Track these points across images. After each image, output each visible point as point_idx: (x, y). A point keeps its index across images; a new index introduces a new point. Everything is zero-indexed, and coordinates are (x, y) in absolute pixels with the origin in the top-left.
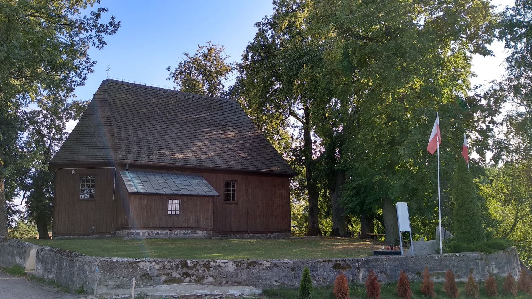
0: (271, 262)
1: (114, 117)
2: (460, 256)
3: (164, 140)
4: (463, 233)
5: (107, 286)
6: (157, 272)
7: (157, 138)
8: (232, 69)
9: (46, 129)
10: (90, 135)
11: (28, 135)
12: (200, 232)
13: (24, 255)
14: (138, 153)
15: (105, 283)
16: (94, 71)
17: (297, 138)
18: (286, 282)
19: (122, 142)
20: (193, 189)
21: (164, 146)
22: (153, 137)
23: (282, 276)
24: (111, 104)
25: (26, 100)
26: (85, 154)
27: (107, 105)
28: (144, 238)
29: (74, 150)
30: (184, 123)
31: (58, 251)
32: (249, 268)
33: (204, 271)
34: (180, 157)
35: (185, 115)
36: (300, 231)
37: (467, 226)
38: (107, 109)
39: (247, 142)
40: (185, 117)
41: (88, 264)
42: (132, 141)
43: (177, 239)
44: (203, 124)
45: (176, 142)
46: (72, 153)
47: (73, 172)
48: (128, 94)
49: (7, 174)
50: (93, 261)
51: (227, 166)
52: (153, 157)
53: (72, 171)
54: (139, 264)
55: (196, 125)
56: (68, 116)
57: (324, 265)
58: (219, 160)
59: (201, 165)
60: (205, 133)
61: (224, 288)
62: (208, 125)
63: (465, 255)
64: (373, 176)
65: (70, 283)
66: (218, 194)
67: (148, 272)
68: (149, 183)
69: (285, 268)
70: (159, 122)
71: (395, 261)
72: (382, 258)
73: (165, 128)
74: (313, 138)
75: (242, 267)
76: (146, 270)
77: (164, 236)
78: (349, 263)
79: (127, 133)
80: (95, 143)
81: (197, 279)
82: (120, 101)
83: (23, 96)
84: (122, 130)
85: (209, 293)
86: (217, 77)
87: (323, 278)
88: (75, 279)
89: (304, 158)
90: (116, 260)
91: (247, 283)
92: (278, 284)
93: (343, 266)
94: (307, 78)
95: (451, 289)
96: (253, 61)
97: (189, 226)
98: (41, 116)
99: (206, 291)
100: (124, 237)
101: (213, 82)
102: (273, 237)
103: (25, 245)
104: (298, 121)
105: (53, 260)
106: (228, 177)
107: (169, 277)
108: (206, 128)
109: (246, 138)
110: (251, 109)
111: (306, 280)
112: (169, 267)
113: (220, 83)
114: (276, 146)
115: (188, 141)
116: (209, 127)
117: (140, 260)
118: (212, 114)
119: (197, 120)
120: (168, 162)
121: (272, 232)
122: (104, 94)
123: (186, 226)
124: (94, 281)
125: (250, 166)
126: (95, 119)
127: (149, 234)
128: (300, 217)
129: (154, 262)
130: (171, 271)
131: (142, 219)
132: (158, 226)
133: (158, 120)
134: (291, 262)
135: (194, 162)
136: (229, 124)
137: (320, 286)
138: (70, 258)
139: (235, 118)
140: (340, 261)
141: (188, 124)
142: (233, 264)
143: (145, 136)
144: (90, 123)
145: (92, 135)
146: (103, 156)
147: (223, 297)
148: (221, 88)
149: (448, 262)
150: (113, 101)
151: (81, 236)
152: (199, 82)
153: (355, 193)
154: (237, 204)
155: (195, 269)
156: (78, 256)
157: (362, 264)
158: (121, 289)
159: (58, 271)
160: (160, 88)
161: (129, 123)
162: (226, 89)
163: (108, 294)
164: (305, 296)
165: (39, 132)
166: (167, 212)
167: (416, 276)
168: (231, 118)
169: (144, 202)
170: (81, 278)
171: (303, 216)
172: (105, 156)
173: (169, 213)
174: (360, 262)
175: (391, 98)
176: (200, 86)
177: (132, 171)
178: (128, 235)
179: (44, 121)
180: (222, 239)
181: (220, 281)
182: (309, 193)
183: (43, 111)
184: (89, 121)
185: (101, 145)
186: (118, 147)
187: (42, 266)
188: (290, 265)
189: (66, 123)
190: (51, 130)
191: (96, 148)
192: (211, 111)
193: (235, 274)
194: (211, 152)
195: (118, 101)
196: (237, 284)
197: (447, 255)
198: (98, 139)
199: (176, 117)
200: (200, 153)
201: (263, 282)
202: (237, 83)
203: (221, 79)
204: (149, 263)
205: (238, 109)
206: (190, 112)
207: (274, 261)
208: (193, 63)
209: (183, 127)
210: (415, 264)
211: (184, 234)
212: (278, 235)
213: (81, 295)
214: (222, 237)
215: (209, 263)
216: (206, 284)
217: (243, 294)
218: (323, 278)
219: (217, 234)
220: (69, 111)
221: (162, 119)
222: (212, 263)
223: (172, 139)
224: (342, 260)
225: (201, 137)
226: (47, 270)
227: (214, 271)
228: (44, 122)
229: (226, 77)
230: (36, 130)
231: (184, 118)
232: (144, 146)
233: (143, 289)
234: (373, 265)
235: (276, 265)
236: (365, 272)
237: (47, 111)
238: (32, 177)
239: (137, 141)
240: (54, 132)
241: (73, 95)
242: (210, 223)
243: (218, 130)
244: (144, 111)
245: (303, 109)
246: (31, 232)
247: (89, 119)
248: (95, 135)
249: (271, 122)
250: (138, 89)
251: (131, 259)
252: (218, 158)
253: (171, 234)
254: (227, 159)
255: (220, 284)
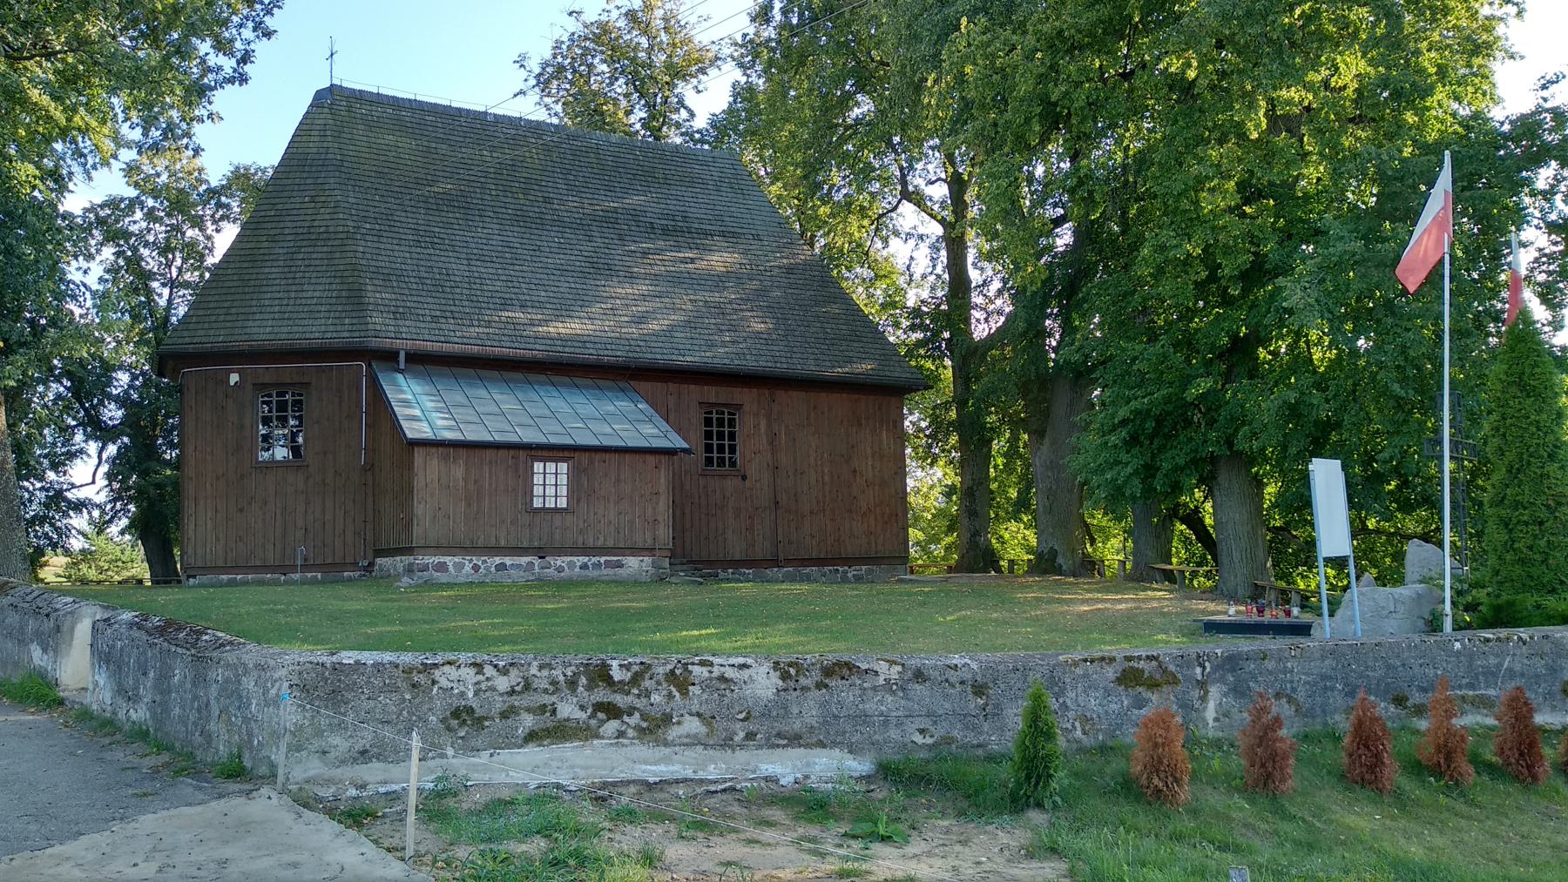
0: (903, 665)
1: (355, 206)
2: (1531, 638)
3: (514, 279)
4: (1522, 561)
5: (324, 753)
6: (504, 702)
7: (491, 270)
8: (717, 58)
9: (154, 254)
10: (281, 263)
11: (102, 273)
12: (633, 563)
13: (54, 637)
14: (435, 319)
15: (317, 744)
16: (275, 31)
17: (924, 277)
18: (955, 733)
19: (381, 283)
20: (608, 430)
21: (514, 296)
22: (478, 269)
23: (940, 712)
24: (346, 164)
25: (82, 160)
26: (270, 323)
27: (332, 168)
28: (461, 580)
29: (233, 311)
30: (574, 226)
31: (157, 627)
32: (826, 686)
33: (670, 696)
34: (563, 331)
35: (574, 199)
36: (929, 557)
37: (1535, 536)
38: (332, 180)
39: (770, 283)
40: (575, 204)
41: (255, 673)
42: (412, 280)
43: (564, 585)
44: (633, 228)
45: (551, 283)
46: (229, 318)
47: (234, 378)
48: (398, 133)
49: (9, 378)
50: (272, 663)
51: (710, 361)
52: (481, 330)
53: (232, 375)
54: (437, 673)
55: (612, 230)
56: (221, 213)
57: (1086, 676)
58: (684, 341)
59: (630, 355)
60: (638, 255)
61: (741, 755)
62: (649, 230)
63: (1548, 636)
64: (1186, 381)
65: (198, 739)
66: (685, 445)
67: (469, 703)
68: (481, 428)
69: (953, 686)
70: (495, 221)
71: (1323, 658)
72: (1280, 650)
73: (513, 240)
74: (975, 276)
75: (803, 681)
76: (462, 694)
77: (522, 573)
78: (1172, 668)
79: (396, 254)
80: (298, 288)
81: (645, 725)
82: (373, 156)
83: (73, 146)
84: (383, 246)
85: (689, 773)
86: (671, 85)
87: (1085, 719)
88: (212, 726)
89: (946, 335)
90: (352, 662)
91: (821, 737)
92: (929, 741)
93: (1151, 677)
94: (975, 64)
95: (1522, 754)
96: (785, 26)
97: (600, 543)
98: (139, 215)
99: (677, 767)
100: (398, 577)
101: (659, 100)
102: (854, 575)
103: (58, 606)
104: (927, 218)
105: (142, 659)
106: (713, 394)
107: (547, 721)
108: (643, 240)
109: (768, 274)
110: (779, 184)
111: (1038, 727)
112: (544, 685)
113: (681, 103)
114: (859, 295)
115: (587, 281)
116: (652, 236)
117: (439, 659)
118: (660, 196)
119: (615, 215)
120: (528, 346)
121: (850, 561)
122: (322, 133)
123: (590, 543)
124: (276, 736)
125: (784, 360)
126: (295, 212)
127: (476, 568)
128: (930, 517)
129: (492, 668)
130: (554, 699)
131: (454, 522)
132: (503, 543)
133: (491, 214)
134: (974, 666)
135: (609, 347)
136: (713, 228)
137: (1075, 746)
138: (193, 651)
139: (732, 209)
140: (1139, 658)
141: (586, 228)
142: (772, 671)
143: (454, 266)
144: (282, 225)
145: (288, 263)
146: (323, 328)
147: (739, 787)
148: (684, 121)
149: (1493, 661)
150: (351, 153)
151: (269, 576)
152: (616, 102)
153: (1124, 437)
154: (744, 478)
155: (636, 692)
156: (222, 645)
157: (1215, 669)
158: (375, 765)
159: (158, 698)
160: (495, 115)
161: (404, 225)
162: (701, 122)
163: (329, 782)
164: (1037, 783)
165: (134, 263)
166: (528, 500)
167: (1392, 708)
168: (721, 208)
169: (458, 471)
170: (232, 724)
171: (941, 514)
172: (331, 328)
173: (537, 503)
174: (1207, 664)
175: (1262, 119)
176: (621, 114)
177: (416, 375)
178: (410, 570)
179: (149, 230)
180: (701, 583)
181: (725, 730)
182: (961, 441)
183: (143, 198)
184: (276, 219)
185: (317, 294)
186: (372, 300)
187: (109, 678)
188: (970, 676)
189: (214, 234)
190: (170, 256)
191: (304, 302)
192: (656, 185)
193: (776, 709)
194: (659, 316)
195: (367, 155)
196: (785, 742)
197: (1491, 636)
198: (307, 275)
199: (548, 206)
200: (626, 319)
201: (875, 732)
202: (735, 101)
203: (685, 90)
204: (472, 671)
205: (741, 181)
206: (590, 191)
207: (914, 663)
208: (597, 39)
209: (570, 236)
210: (1389, 667)
211: (584, 567)
212: (869, 572)
213: (233, 786)
214: (702, 577)
215: (686, 670)
216: (678, 741)
217: (806, 777)
218: (1085, 719)
219: (685, 567)
220: (223, 199)
221: (504, 210)
222: (696, 670)
223: (538, 276)
224: (1148, 657)
225: (626, 269)
226: (127, 694)
227: (705, 696)
228: (149, 232)
229: (699, 82)
230: (127, 259)
231: (574, 210)
232: (450, 296)
233: (454, 761)
234: (1250, 672)
235: (920, 676)
236: (1225, 695)
237: (155, 198)
238: (122, 401)
239: (429, 282)
240: (178, 262)
241: (210, 116)
242: (664, 533)
243: (679, 248)
244: (449, 186)
245: (945, 181)
246: (129, 565)
247: (278, 213)
248: (300, 263)
249: (845, 221)
250: (427, 118)
251: (407, 658)
252: (682, 335)
253: (542, 568)
254: (711, 338)
255: (727, 743)
